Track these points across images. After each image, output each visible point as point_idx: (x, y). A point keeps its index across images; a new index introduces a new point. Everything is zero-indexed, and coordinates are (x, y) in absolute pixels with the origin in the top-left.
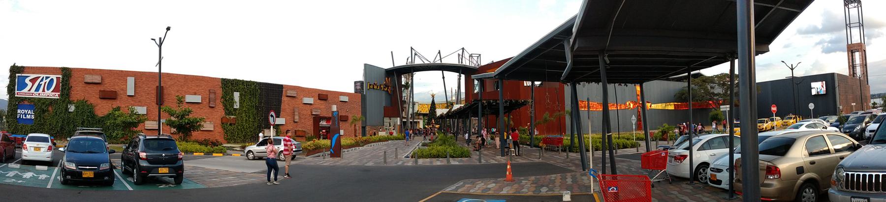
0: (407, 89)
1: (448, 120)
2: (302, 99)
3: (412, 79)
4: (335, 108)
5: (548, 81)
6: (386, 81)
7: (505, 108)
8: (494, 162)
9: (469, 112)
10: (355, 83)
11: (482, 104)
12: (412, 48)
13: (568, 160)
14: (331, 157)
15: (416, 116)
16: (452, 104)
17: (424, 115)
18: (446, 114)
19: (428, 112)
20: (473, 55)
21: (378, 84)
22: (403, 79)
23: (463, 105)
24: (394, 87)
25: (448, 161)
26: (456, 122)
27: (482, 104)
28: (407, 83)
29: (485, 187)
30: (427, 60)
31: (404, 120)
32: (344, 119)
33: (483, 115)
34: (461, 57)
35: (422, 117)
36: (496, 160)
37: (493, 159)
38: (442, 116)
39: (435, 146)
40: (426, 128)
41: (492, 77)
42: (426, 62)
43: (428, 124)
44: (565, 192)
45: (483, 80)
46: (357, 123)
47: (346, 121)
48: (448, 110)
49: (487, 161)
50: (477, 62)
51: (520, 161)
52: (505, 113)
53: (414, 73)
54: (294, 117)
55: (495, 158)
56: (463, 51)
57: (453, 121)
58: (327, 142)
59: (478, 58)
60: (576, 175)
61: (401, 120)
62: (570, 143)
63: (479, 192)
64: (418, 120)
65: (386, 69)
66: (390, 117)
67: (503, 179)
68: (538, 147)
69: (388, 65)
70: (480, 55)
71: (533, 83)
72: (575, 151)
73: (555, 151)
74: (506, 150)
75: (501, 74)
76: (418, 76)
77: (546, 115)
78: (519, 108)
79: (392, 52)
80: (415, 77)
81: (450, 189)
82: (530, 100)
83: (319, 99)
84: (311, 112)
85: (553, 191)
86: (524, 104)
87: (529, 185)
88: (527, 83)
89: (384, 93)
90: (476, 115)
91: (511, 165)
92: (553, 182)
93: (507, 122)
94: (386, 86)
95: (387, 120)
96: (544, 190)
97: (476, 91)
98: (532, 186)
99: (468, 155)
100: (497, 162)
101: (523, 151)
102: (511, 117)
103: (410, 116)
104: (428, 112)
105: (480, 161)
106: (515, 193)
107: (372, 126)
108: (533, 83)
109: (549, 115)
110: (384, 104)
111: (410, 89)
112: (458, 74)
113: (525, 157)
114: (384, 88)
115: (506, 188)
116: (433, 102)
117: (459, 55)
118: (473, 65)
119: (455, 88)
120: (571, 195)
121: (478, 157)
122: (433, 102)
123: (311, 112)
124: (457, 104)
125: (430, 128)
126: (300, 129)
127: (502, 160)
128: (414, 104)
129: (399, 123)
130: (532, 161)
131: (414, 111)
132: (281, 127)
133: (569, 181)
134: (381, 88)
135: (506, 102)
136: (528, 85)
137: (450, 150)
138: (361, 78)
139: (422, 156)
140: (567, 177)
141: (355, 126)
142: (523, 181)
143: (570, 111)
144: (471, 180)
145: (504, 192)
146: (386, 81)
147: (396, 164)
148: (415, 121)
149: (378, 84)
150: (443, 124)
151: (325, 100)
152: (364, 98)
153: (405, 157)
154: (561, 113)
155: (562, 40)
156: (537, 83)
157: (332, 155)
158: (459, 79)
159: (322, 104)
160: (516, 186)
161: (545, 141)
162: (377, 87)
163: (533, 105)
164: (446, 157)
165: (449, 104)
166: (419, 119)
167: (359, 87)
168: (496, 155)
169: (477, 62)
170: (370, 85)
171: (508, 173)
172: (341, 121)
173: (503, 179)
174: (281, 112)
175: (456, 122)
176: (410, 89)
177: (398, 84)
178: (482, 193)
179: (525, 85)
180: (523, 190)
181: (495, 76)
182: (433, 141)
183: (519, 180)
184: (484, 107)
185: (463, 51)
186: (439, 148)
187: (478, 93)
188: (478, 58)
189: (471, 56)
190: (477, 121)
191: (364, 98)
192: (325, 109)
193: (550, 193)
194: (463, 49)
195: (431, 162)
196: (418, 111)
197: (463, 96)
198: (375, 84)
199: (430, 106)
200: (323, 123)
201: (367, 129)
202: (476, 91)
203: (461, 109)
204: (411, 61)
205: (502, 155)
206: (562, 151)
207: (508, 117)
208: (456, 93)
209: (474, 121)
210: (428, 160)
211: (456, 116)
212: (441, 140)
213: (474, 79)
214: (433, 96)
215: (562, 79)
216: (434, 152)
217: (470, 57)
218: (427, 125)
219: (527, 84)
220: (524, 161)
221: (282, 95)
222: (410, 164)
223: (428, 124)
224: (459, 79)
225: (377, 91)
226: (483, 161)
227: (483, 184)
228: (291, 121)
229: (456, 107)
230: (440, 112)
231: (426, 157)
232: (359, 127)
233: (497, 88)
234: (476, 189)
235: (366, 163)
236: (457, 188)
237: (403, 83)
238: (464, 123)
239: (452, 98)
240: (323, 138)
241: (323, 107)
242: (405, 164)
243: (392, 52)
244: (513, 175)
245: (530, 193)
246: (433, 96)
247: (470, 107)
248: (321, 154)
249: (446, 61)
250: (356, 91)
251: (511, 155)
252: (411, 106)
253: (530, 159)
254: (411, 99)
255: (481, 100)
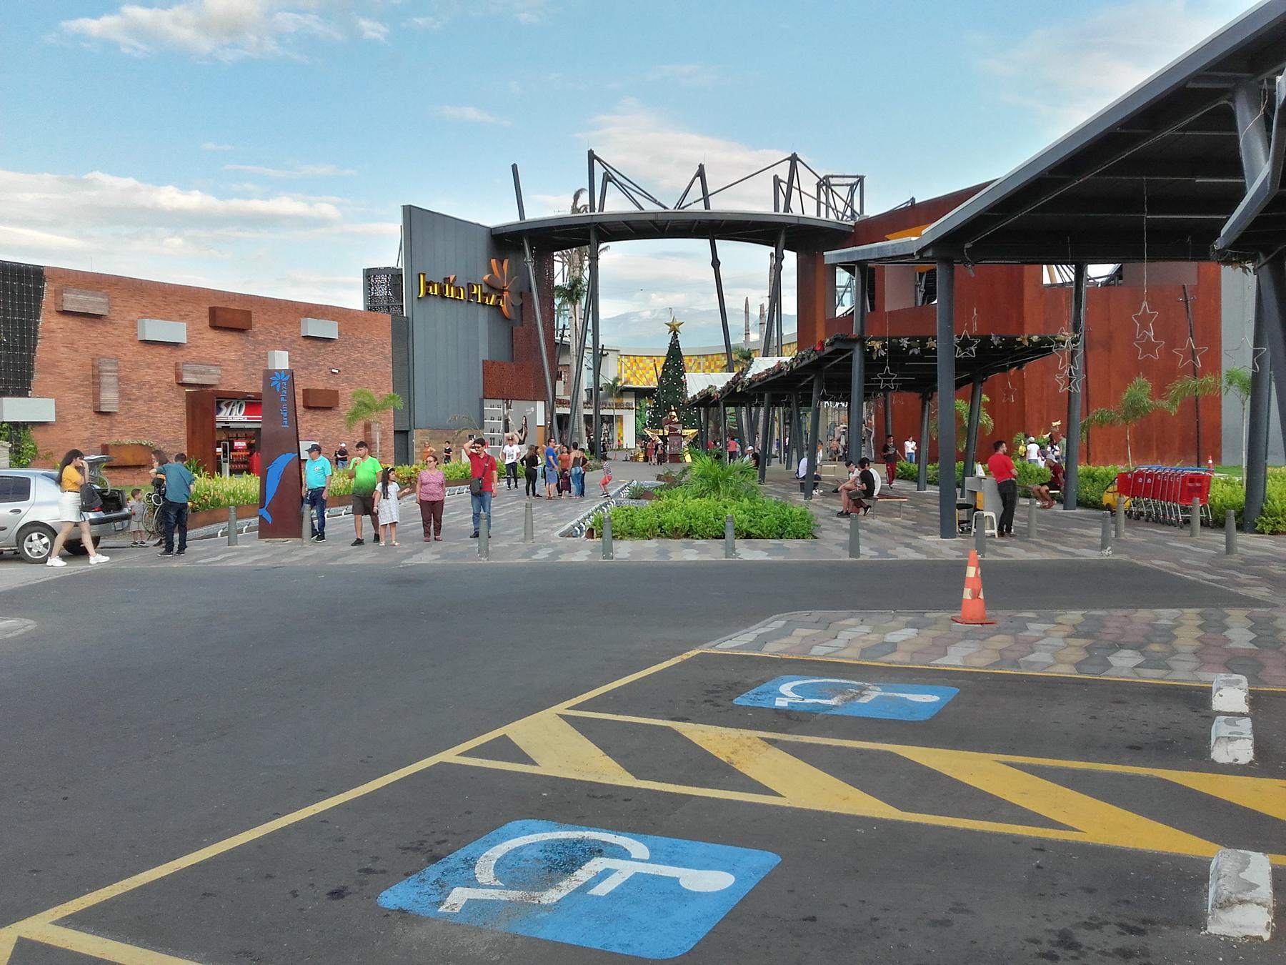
0: (574, 303)
1: (731, 410)
2: (134, 325)
3: (594, 268)
4: (281, 360)
5: (1150, 260)
6: (490, 270)
7: (961, 365)
8: (911, 555)
9: (812, 381)
10: (370, 274)
11: (868, 355)
12: (592, 157)
13: (1235, 559)
14: (261, 536)
15: (610, 396)
16: (747, 357)
17: (640, 393)
18: (723, 391)
19: (654, 384)
20: (833, 181)
21: (462, 282)
22: (558, 267)
23: (788, 359)
24: (525, 295)
25: (731, 550)
26: (761, 418)
27: (868, 355)
28: (576, 282)
29: (874, 638)
30: (655, 201)
31: (560, 410)
32: (322, 403)
33: (868, 393)
34: (785, 188)
35: (632, 401)
36: (918, 549)
37: (908, 546)
38: (706, 400)
39: (680, 497)
40: (646, 438)
41: (912, 255)
42: (650, 207)
43: (656, 423)
44: (1222, 676)
45: (873, 270)
46: (373, 417)
47: (330, 408)
48: (733, 375)
49: (882, 552)
50: (849, 204)
51: (1015, 552)
52: (958, 385)
53: (602, 246)
54: (96, 396)
55: (914, 542)
56: (793, 169)
57: (749, 413)
58: (249, 484)
59: (852, 192)
60: (1275, 618)
61: (550, 410)
62: (1240, 496)
63: (850, 656)
64: (618, 412)
65: (491, 230)
66: (507, 398)
67: (950, 616)
68: (1096, 505)
69: (502, 215)
70: (861, 179)
71: (1080, 273)
72: (1267, 529)
73: (1171, 524)
74: (961, 514)
75: (948, 246)
76: (614, 255)
77: (1140, 389)
78: (1020, 366)
79: (515, 168)
80: (604, 258)
81: (734, 643)
82: (1067, 336)
83: (214, 327)
84: (178, 376)
85: (1168, 668)
86: (1042, 349)
87: (1061, 643)
88: (1057, 275)
89: (483, 316)
90: (840, 389)
91: (982, 565)
92: (1168, 635)
93: (966, 419)
94: (492, 288)
95: (494, 409)
96: (1124, 665)
97: (840, 311)
98: (1069, 645)
99: (804, 530)
100: (923, 557)
101: (1034, 521)
102: (985, 398)
103: (584, 397)
104: (654, 384)
105: (854, 549)
106: (994, 665)
107: (436, 430)
108: (1080, 273)
109: (1148, 390)
110: (484, 354)
111: (584, 300)
112: (773, 250)
113: (1042, 541)
114: (484, 295)
115: (962, 644)
116: (675, 353)
117: (777, 182)
118: (832, 217)
119: (760, 298)
120: (1251, 692)
121: (846, 537)
122: (675, 353)
123: (178, 376)
124: (766, 355)
125: (662, 438)
126: (127, 440)
127: (945, 550)
128: (599, 355)
129: (541, 421)
130: (1069, 557)
131: (602, 381)
132: (35, 434)
133: (1240, 636)
134: (471, 296)
135: (965, 344)
136: (1059, 281)
137: (736, 512)
138: (390, 257)
139: (631, 532)
140: (1228, 621)
141: (367, 427)
142: (1032, 626)
143: (1248, 372)
144: (817, 614)
145: (955, 658)
146: (490, 270)
147: (524, 556)
148: (603, 412)
149: (462, 282)
150: (711, 425)
151: (241, 330)
152: (402, 333)
153: (562, 535)
154: (1209, 379)
155: (1223, 92)
156: (1099, 271)
157: (266, 531)
158: (777, 269)
159: (227, 348)
160: (1001, 641)
161: (1127, 484)
162: (458, 292)
163: (1081, 351)
164: (723, 537)
165: (735, 357)
166: (619, 406)
167: (382, 292)
168: (919, 529)
169: (849, 204)
170: (428, 284)
171: (967, 594)
172: (308, 407)
173: (950, 616)
174: (36, 376)
175: (761, 418)
176: (584, 300)
177: (537, 284)
178: (862, 656)
179: (1046, 280)
180: (1032, 658)
181: (920, 252)
182: (671, 483)
183: (1012, 619)
184: (872, 365)
185: (793, 169)
186: (694, 504)
187: (849, 317)
188: (852, 192)
189: (824, 184)
190: (844, 415)
191: (402, 333)
192: (241, 365)
193: (1152, 676)
194: (794, 159)
195: (664, 552)
196: (617, 379)
197: (790, 329)
198: (446, 280)
199: (663, 360)
200: (234, 416)
201: (417, 438)
202: (840, 311)
203: (781, 371)
204: (588, 203)
205: (947, 532)
206: (1204, 524)
207: (972, 398)
208: (762, 316)
209: (834, 414)
210: (653, 544)
211: (761, 398)
212: (703, 476)
213: (834, 267)
214: (675, 331)
215: (1219, 244)
216: (675, 517)
217: (819, 186)
218: (651, 425)
219: (1051, 276)
220: (1036, 556)
221: (38, 308)
222: (581, 557)
223: (656, 423)
224: (777, 269)
225: (454, 304)
226: (867, 552)
227: (866, 629)
228: (82, 411)
229: (761, 365)
230: (696, 383)
231: (645, 534)
232: (384, 433)
233: (930, 294)
234: (840, 642)
235: (409, 555)
236: (762, 640)
237: (558, 281)
238: (792, 421)
239: (747, 334)
240: (232, 472)
241: (233, 355)
242: (564, 558)
243: (515, 168)
244: (990, 602)
245: (1064, 670)
246: (675, 331)
247: (816, 366)
248: (219, 528)
249: (723, 205)
250: (372, 303)
251: (980, 534)
252: (588, 361)
253: (1060, 547)
254: (589, 336)
255: (861, 340)
